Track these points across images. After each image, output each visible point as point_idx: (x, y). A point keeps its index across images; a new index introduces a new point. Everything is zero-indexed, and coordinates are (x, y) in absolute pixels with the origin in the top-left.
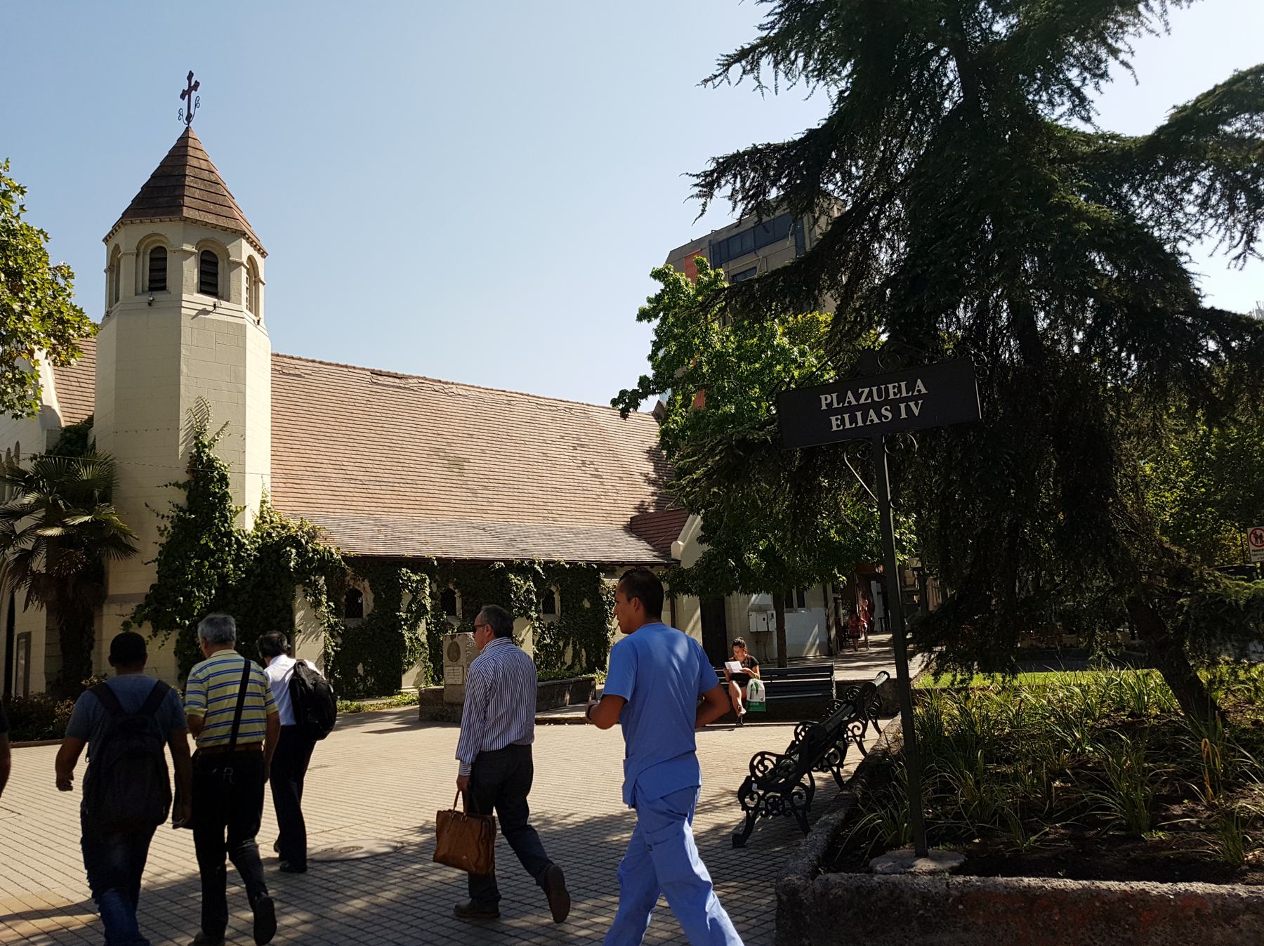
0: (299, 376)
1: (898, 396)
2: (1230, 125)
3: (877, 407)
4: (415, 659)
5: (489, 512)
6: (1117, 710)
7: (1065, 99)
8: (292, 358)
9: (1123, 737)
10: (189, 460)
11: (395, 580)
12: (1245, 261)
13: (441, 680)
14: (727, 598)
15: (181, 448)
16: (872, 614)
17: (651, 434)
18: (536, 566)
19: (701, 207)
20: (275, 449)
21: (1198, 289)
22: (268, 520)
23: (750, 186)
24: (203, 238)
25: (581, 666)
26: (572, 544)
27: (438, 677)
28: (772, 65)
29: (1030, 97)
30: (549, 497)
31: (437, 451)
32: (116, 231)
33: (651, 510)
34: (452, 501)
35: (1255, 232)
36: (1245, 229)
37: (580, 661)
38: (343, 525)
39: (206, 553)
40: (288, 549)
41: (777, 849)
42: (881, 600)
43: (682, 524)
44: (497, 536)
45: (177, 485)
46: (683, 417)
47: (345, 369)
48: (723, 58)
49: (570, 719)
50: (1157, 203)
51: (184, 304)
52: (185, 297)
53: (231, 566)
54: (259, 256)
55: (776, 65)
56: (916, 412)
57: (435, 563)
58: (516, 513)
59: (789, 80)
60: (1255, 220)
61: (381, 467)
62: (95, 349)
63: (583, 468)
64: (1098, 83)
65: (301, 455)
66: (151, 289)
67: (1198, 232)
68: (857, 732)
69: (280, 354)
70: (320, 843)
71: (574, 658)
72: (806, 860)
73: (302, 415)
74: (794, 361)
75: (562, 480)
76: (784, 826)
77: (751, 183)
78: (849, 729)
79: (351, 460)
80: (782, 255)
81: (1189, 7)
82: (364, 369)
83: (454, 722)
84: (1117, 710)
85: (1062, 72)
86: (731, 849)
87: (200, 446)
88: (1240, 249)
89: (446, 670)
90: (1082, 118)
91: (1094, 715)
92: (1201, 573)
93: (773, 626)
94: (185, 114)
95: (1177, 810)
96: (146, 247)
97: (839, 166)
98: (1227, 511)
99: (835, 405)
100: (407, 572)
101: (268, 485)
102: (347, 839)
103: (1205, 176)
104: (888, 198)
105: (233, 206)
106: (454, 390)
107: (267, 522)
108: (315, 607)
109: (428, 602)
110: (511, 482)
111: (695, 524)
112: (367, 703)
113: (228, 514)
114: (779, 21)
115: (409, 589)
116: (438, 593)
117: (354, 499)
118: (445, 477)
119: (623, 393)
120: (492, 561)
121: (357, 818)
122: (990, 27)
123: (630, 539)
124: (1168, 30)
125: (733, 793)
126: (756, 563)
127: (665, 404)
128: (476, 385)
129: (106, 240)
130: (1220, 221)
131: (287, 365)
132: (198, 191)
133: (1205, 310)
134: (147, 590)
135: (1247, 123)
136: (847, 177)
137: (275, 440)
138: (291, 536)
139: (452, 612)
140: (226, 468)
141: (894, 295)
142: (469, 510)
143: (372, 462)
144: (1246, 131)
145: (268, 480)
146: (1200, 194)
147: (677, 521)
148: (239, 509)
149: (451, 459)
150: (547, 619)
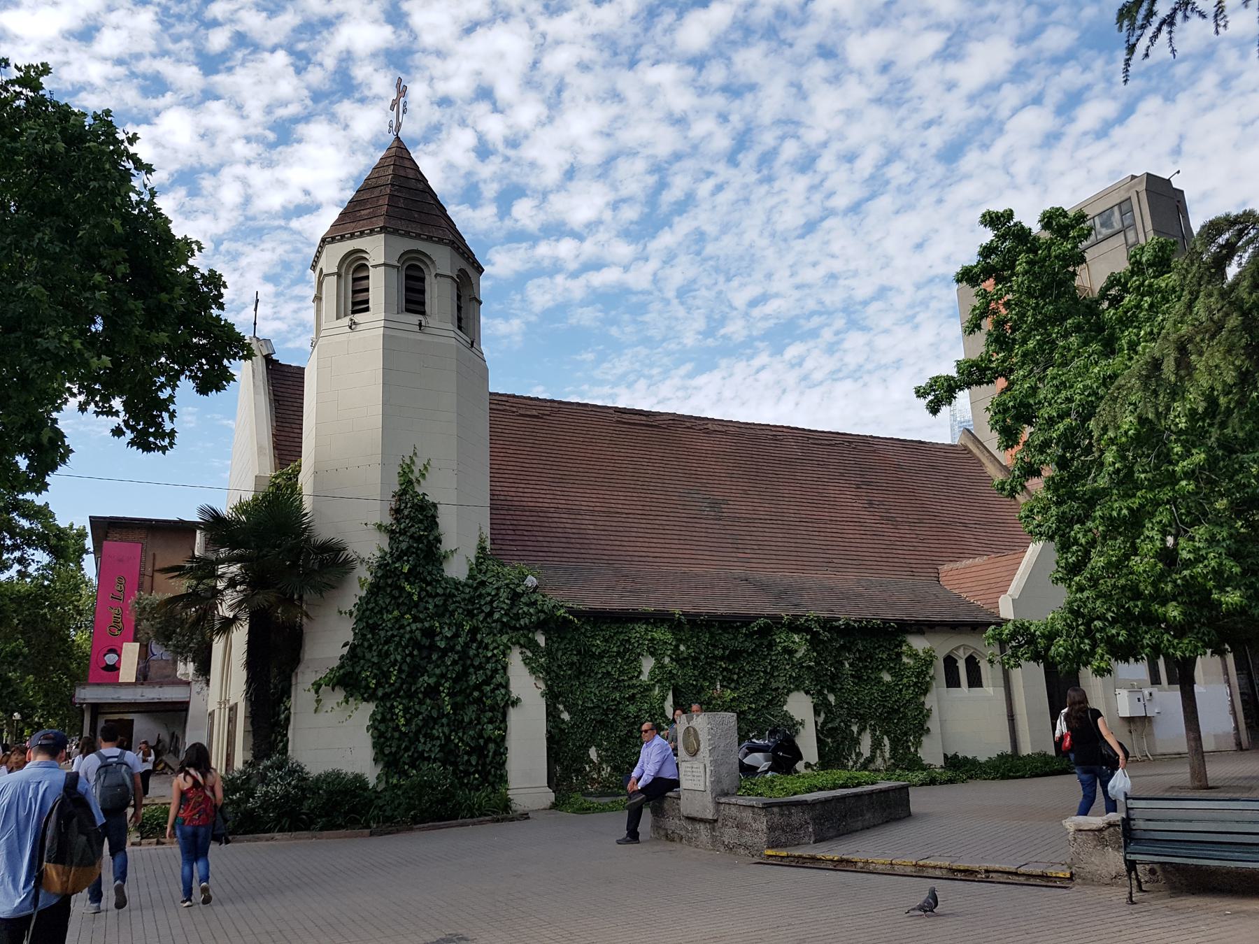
37: (882, 752)
72: (548, 297)
106: (709, 426)
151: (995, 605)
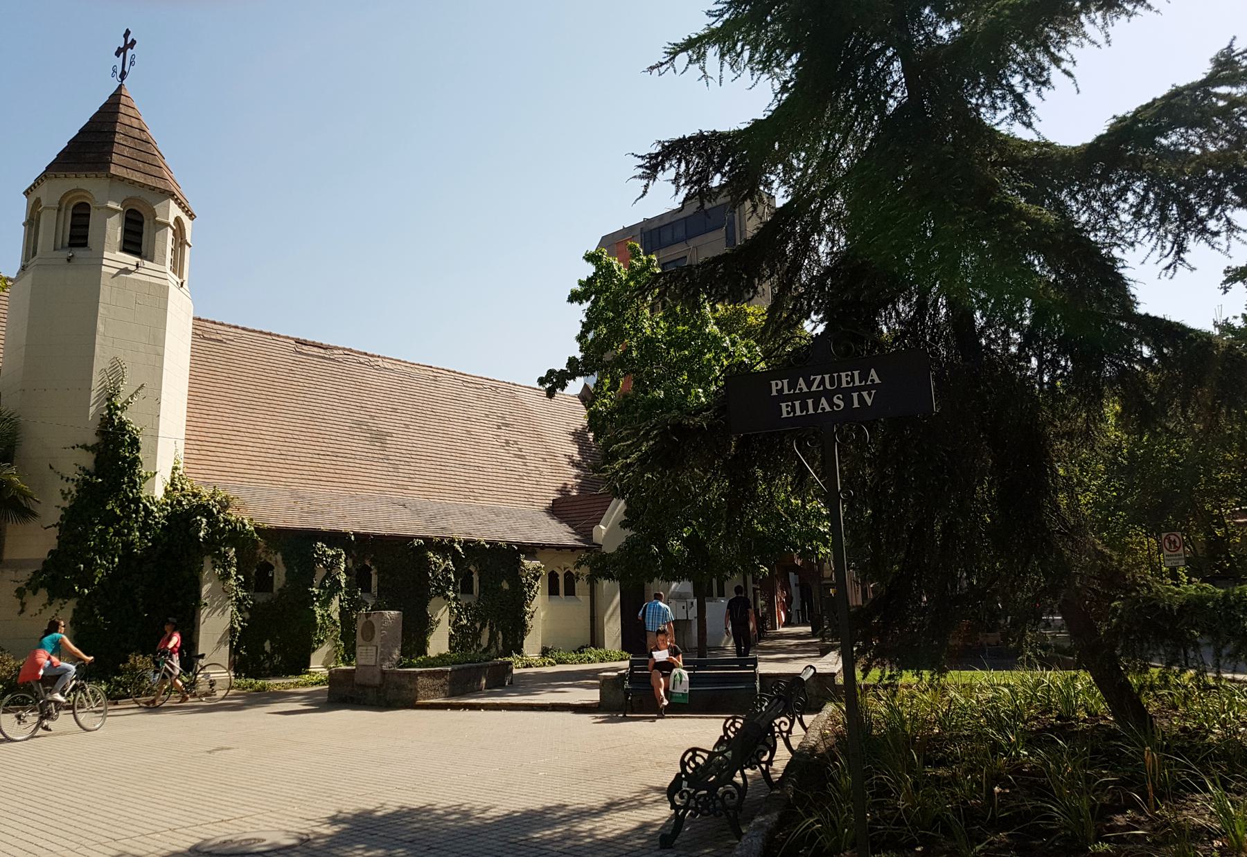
0: (221, 341)
1: (851, 385)
2: (1166, 138)
3: (829, 395)
4: (326, 637)
5: (410, 487)
6: (1043, 713)
7: (1007, 105)
8: (215, 323)
9: (1060, 742)
10: (99, 421)
11: (311, 555)
12: (1175, 271)
13: (352, 660)
14: (647, 585)
15: (92, 410)
16: (789, 606)
17: (579, 417)
18: (456, 545)
19: (643, 189)
20: (191, 414)
21: (1134, 296)
22: (179, 487)
23: (694, 171)
24: (129, 196)
25: (497, 648)
26: (493, 524)
27: (349, 657)
28: (718, 56)
29: (974, 101)
30: (471, 475)
31: (360, 423)
32: (39, 184)
33: (574, 493)
34: (372, 475)
35: (1185, 242)
36: (1176, 240)
37: (496, 643)
38: (257, 495)
39: (111, 519)
40: (198, 518)
41: (707, 851)
42: (799, 591)
43: (605, 508)
44: (418, 513)
45: (85, 447)
46: (612, 400)
47: (269, 337)
48: (670, 46)
49: (487, 704)
50: (1094, 210)
51: (105, 262)
52: (106, 254)
53: (138, 534)
54: (187, 218)
55: (722, 56)
56: (869, 402)
57: (353, 538)
58: (437, 490)
59: (734, 72)
60: (1185, 231)
61: (301, 437)
62: (7, 303)
63: (507, 448)
64: (1040, 89)
65: (217, 422)
66: (71, 245)
67: (1132, 240)
68: (785, 728)
69: (202, 318)
70: (217, 834)
71: (490, 640)
73: (222, 382)
74: (726, 349)
75: (485, 459)
76: (712, 826)
77: (695, 168)
78: (776, 725)
79: (270, 429)
80: (711, 246)
81: (1129, 21)
82: (288, 338)
83: (365, 704)
84: (1043, 713)
85: (1005, 77)
86: (658, 850)
87: (112, 409)
88: (1170, 260)
89: (359, 650)
90: (1024, 123)
91: (1023, 717)
92: (1133, 576)
93: (693, 613)
94: (119, 72)
95: (1120, 820)
96: (69, 202)
97: (781, 157)
98: (1136, 518)
99: (786, 392)
100: (322, 547)
101: (181, 451)
102: (248, 830)
103: (1139, 186)
104: (829, 192)
105: (162, 165)
106: (380, 363)
107: (177, 489)
108: (223, 579)
109: (343, 578)
110: (433, 459)
111: (618, 508)
112: (273, 682)
113: (137, 480)
114: (728, 10)
115: (324, 565)
116: (354, 569)
117: (271, 469)
118: (366, 450)
119: (551, 372)
120: (412, 538)
121: (260, 806)
122: (935, 31)
123: (551, 522)
124: (1108, 42)
125: (658, 789)
126: (679, 550)
127: (592, 387)
128: (402, 360)
129: (27, 193)
130: (1152, 230)
131: (208, 330)
132: (127, 149)
133: (1140, 315)
134: (44, 555)
135: (1182, 136)
136: (789, 169)
137: (191, 406)
138: (202, 505)
139: (367, 589)
140: (138, 431)
141: (834, 284)
142: (389, 485)
143: (291, 432)
144: (1181, 144)
145: (181, 445)
146: (1135, 204)
147: (600, 505)
148: (149, 475)
149: (373, 432)
150: (465, 600)
151: (590, 533)
